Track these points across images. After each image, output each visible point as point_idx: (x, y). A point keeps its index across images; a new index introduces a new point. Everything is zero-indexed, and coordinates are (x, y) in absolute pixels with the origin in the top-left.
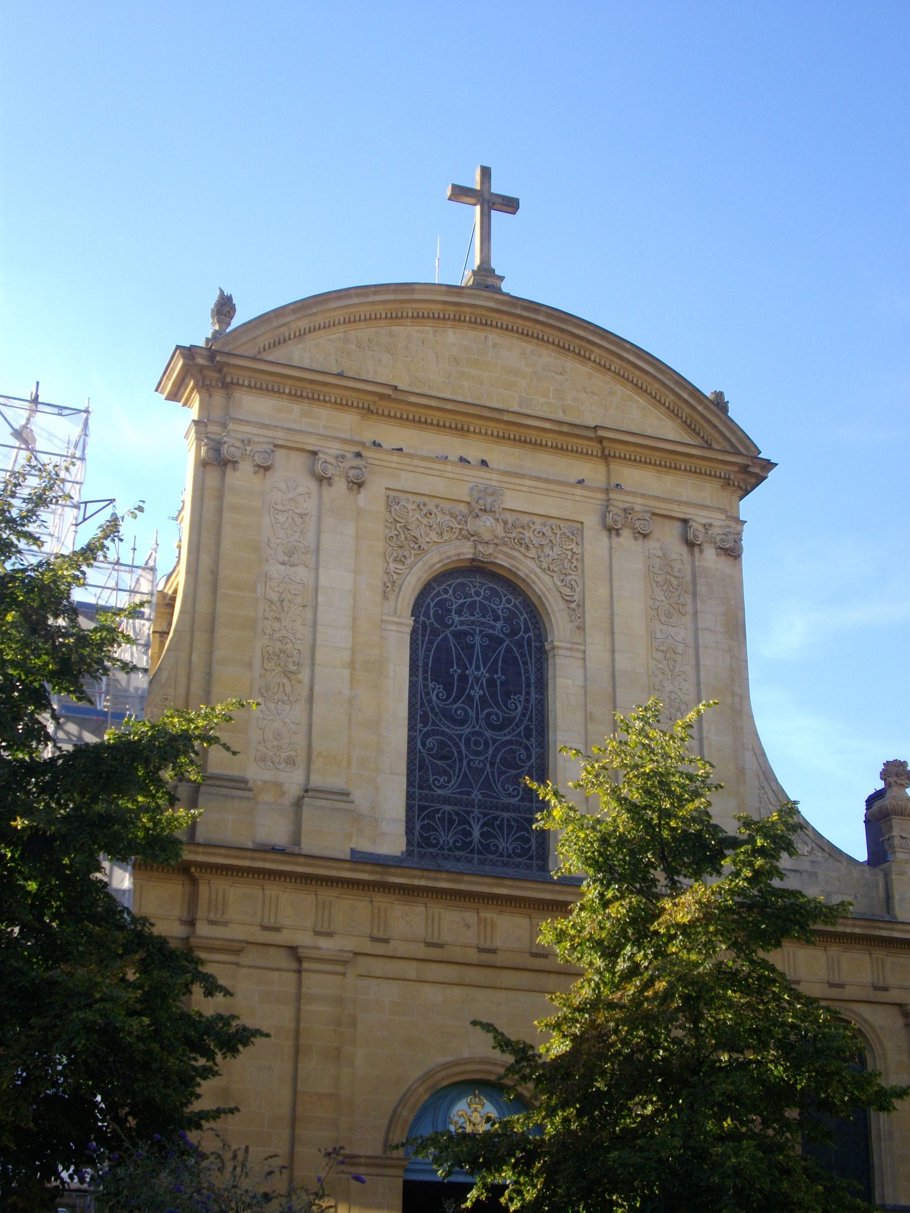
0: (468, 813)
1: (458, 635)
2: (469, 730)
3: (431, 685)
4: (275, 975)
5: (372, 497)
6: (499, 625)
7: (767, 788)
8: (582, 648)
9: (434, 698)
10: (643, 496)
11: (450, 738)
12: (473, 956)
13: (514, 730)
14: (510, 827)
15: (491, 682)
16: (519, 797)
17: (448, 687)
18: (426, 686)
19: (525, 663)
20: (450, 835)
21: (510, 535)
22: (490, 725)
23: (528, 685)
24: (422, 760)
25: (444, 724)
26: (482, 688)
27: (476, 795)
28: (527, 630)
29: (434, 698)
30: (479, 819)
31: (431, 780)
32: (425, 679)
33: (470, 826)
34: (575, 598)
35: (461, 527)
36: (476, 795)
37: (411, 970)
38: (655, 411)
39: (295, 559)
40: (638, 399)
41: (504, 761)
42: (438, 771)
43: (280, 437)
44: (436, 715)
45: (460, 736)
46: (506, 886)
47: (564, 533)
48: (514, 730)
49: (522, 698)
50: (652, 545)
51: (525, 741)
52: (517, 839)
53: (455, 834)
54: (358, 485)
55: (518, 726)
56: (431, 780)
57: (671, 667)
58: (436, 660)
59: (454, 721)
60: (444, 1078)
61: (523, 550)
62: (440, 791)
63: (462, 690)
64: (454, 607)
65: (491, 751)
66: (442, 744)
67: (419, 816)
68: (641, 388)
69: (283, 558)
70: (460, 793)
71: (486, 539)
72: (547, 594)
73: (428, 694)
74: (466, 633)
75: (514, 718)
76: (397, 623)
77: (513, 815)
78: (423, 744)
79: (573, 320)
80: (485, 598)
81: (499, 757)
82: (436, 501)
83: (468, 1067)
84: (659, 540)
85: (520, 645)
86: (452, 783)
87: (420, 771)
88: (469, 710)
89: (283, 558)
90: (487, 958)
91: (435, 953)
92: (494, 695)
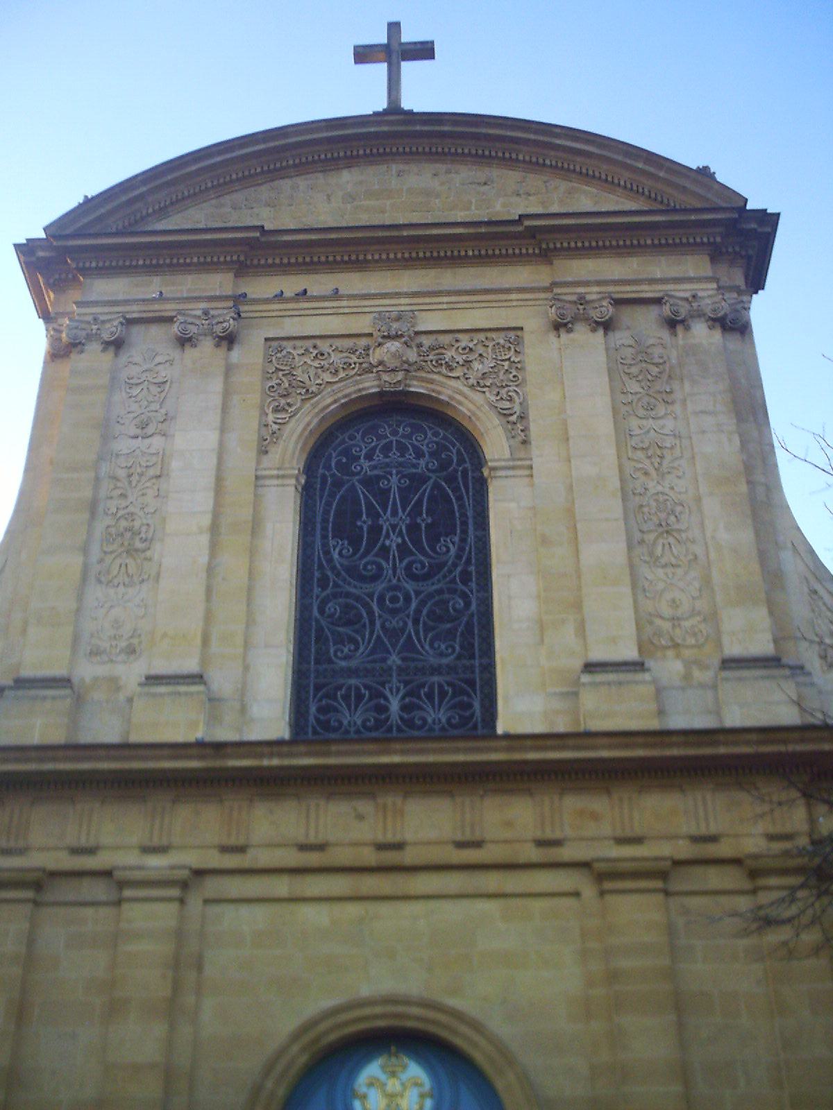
0: (383, 684)
1: (369, 482)
2: (383, 585)
3: (332, 543)
4: (89, 912)
5: (249, 354)
6: (422, 462)
7: (822, 592)
8: (528, 463)
9: (336, 556)
10: (599, 283)
11: (358, 599)
12: (370, 857)
13: (445, 577)
14: (443, 694)
15: (413, 528)
16: (455, 655)
17: (355, 542)
18: (325, 545)
19: (460, 498)
20: (359, 713)
21: (426, 358)
22: (412, 577)
23: (464, 523)
24: (320, 630)
25: (349, 584)
26: (400, 534)
27: (394, 660)
28: (461, 461)
29: (336, 556)
30: (398, 690)
31: (332, 651)
32: (324, 537)
33: (386, 699)
34: (515, 410)
35: (361, 360)
36: (394, 660)
37: (281, 886)
38: (611, 196)
39: (150, 430)
40: (587, 188)
41: (431, 613)
42: (340, 640)
43: (135, 311)
44: (338, 575)
45: (371, 596)
46: (395, 752)
47: (498, 344)
48: (445, 577)
49: (456, 539)
50: (620, 337)
51: (461, 586)
52: (454, 707)
53: (367, 710)
54: (229, 340)
55: (450, 572)
56: (332, 651)
57: (656, 465)
58: (338, 514)
59: (363, 579)
60: (332, 1029)
61: (444, 371)
62: (343, 664)
63: (373, 542)
64: (364, 452)
65: (414, 605)
66: (347, 608)
67: (315, 696)
68: (587, 174)
69: (134, 431)
70: (374, 661)
71: (392, 366)
72: (478, 412)
73: (327, 553)
74: (378, 478)
75: (445, 564)
76: (278, 477)
77: (448, 678)
78: (322, 611)
79: (486, 120)
80: (403, 436)
81: (425, 612)
82: (329, 342)
83: (367, 1011)
84: (628, 328)
85: (451, 480)
86: (361, 650)
87: (316, 642)
88: (384, 563)
89: (134, 431)
90: (390, 857)
91: (313, 859)
92: (417, 543)
